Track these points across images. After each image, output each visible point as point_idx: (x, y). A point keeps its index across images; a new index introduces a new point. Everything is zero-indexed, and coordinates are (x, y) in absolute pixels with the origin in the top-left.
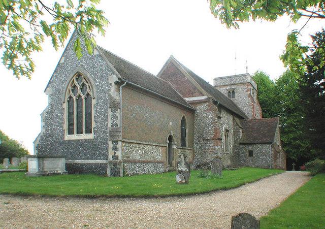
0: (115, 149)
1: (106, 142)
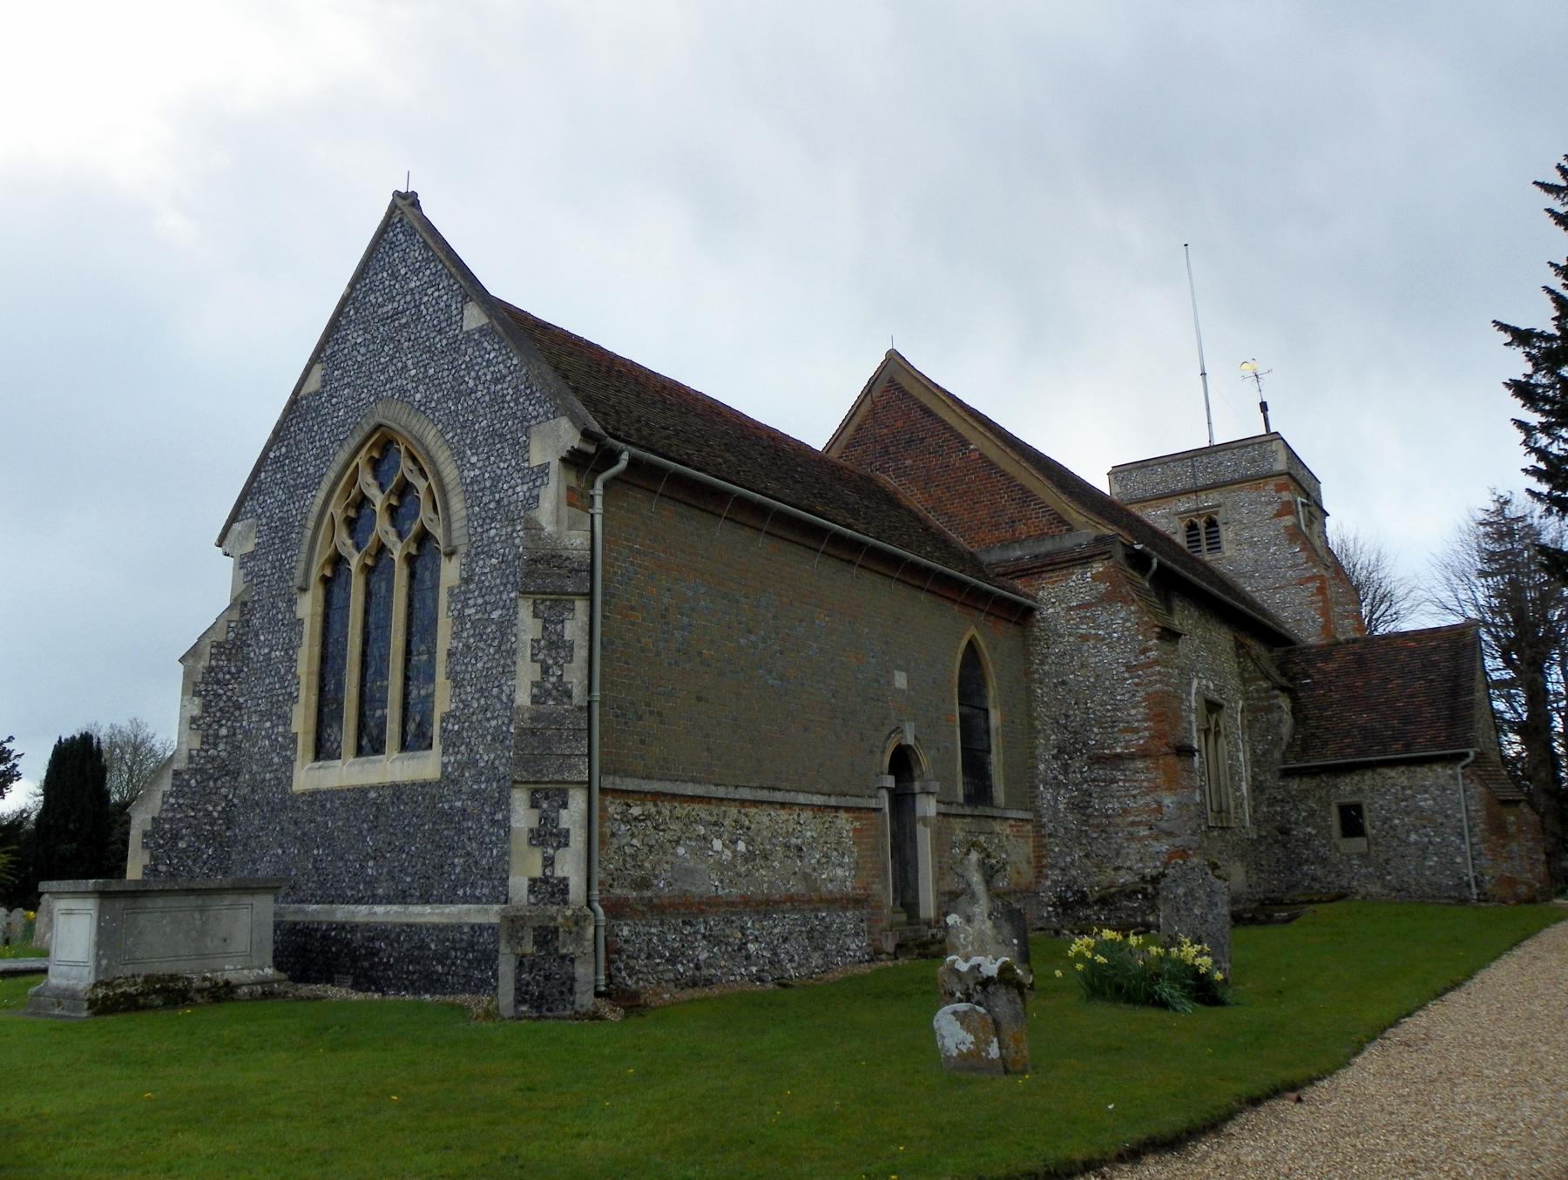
0: (548, 836)
1: (503, 802)
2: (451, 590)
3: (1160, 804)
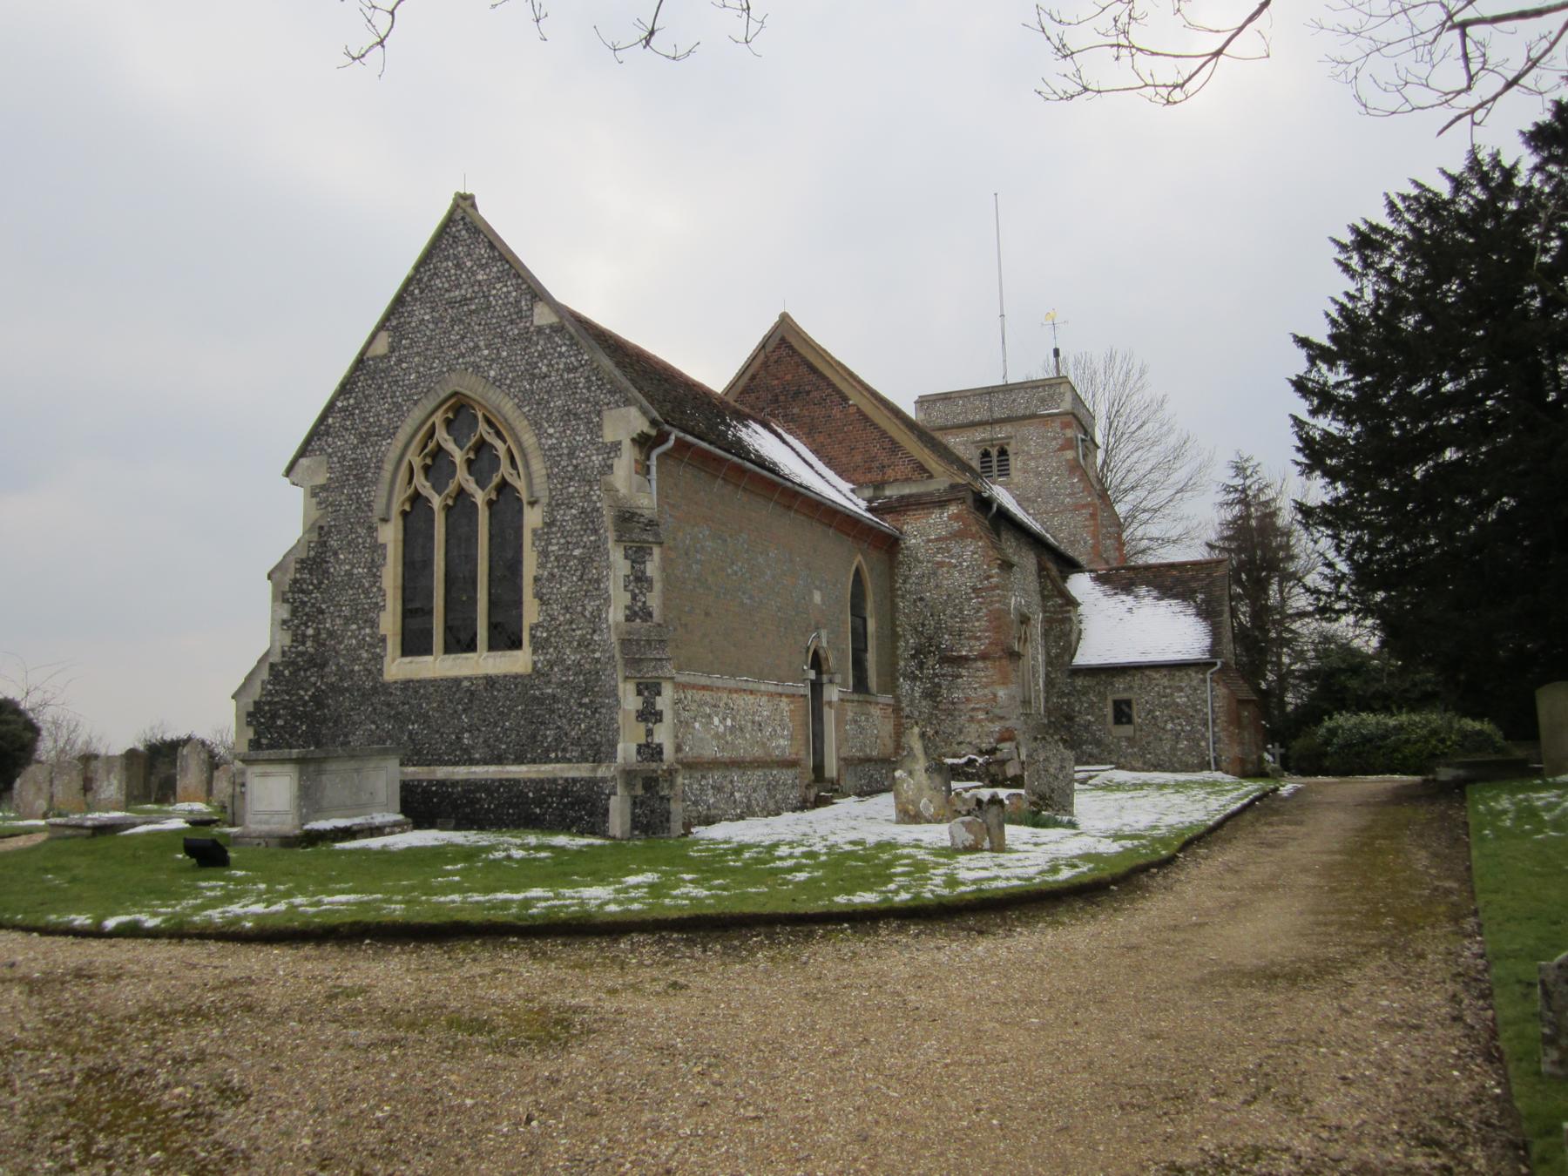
0: (649, 715)
2: (534, 531)
3: (995, 696)
